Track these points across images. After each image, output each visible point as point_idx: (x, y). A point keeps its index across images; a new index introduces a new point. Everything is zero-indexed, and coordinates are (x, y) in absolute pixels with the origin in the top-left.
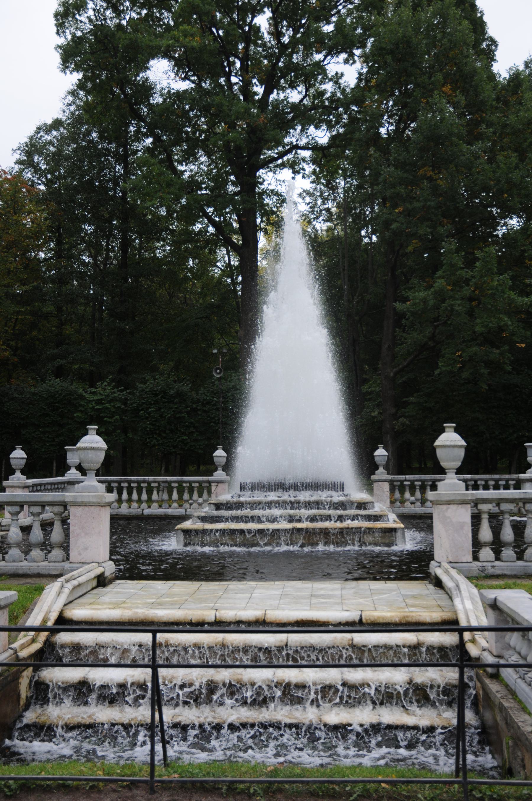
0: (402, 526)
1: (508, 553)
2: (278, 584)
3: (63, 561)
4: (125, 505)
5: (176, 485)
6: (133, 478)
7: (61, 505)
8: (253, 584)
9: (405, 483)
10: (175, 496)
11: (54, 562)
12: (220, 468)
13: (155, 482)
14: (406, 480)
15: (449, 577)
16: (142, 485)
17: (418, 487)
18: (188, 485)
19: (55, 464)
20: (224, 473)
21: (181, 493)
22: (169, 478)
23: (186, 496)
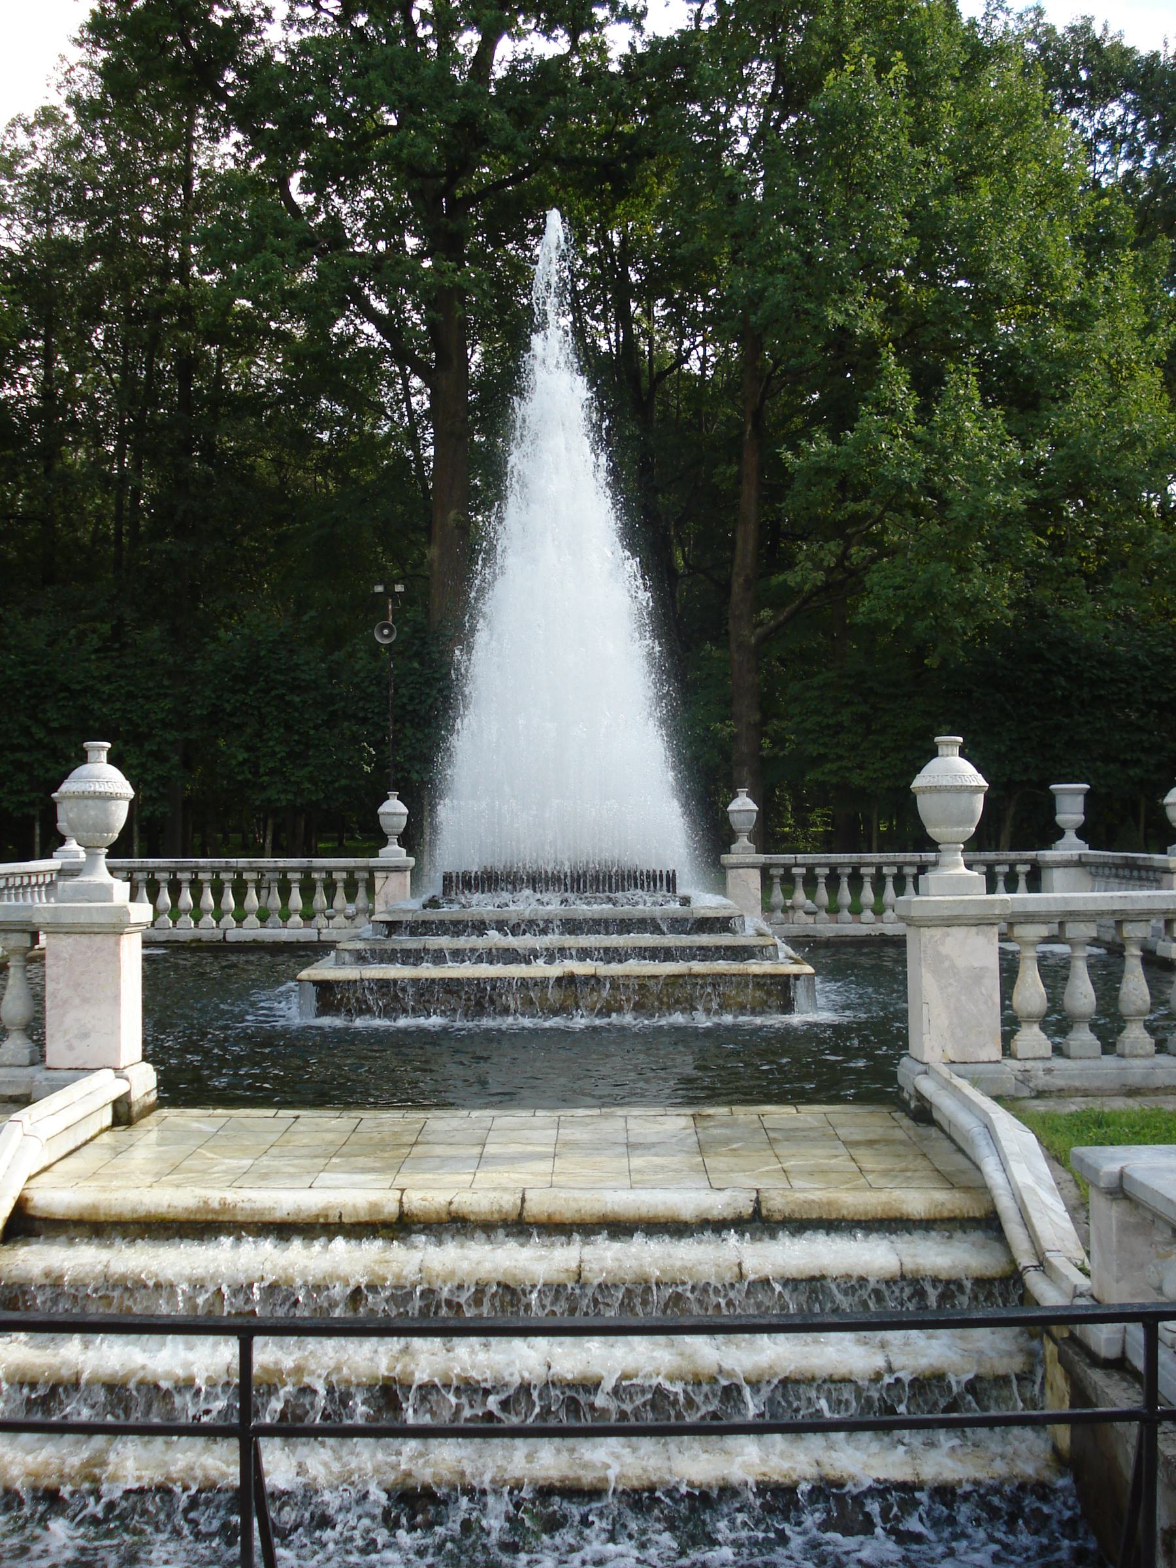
0: (808, 969)
1: (1083, 1038)
2: (543, 1116)
3: (32, 1064)
4: (187, 921)
5: (298, 876)
6: (202, 861)
7: (24, 931)
8: (481, 1116)
9: (795, 870)
10: (296, 900)
11: (11, 1066)
12: (393, 840)
13: (252, 870)
14: (797, 865)
15: (963, 1104)
16: (223, 876)
17: (822, 880)
18: (324, 875)
19: (38, 831)
20: (404, 851)
21: (308, 891)
22: (282, 862)
23: (320, 900)
